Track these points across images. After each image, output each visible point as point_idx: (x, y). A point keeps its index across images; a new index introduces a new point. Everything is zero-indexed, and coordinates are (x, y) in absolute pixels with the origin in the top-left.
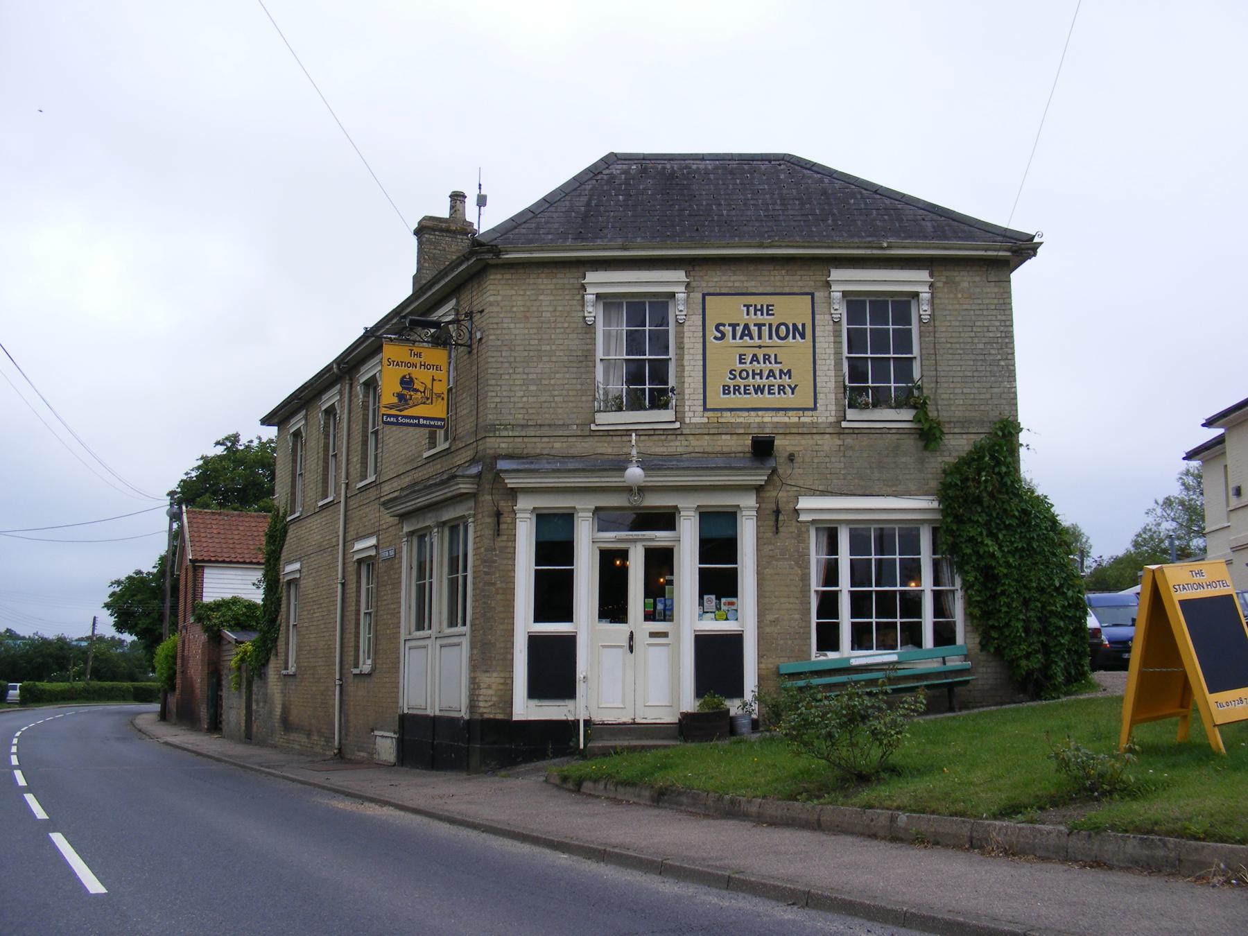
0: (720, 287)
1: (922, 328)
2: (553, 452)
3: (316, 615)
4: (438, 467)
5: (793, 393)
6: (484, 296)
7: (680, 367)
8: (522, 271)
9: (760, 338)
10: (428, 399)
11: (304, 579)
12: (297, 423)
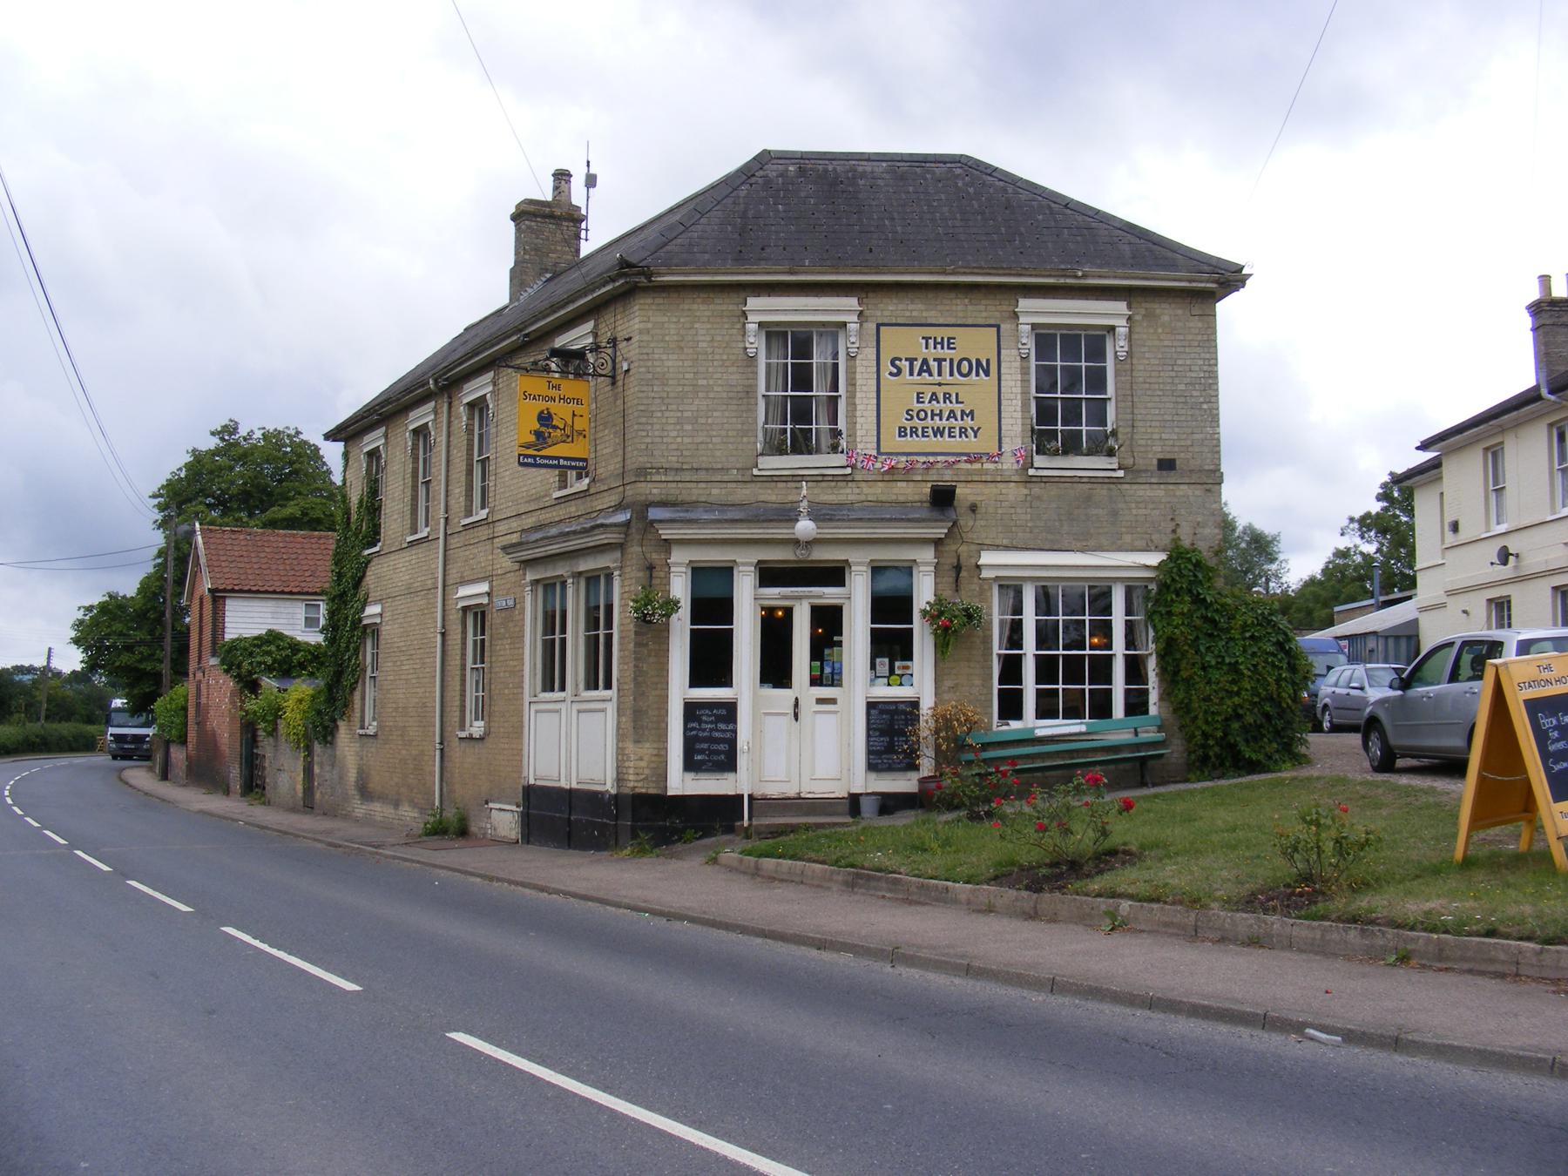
0: (896, 317)
1: (1119, 366)
2: (711, 499)
3: (404, 668)
4: (573, 509)
5: (975, 437)
6: (632, 322)
7: (852, 405)
8: (676, 295)
9: (940, 374)
10: (568, 437)
11: (387, 625)
12: (374, 440)
